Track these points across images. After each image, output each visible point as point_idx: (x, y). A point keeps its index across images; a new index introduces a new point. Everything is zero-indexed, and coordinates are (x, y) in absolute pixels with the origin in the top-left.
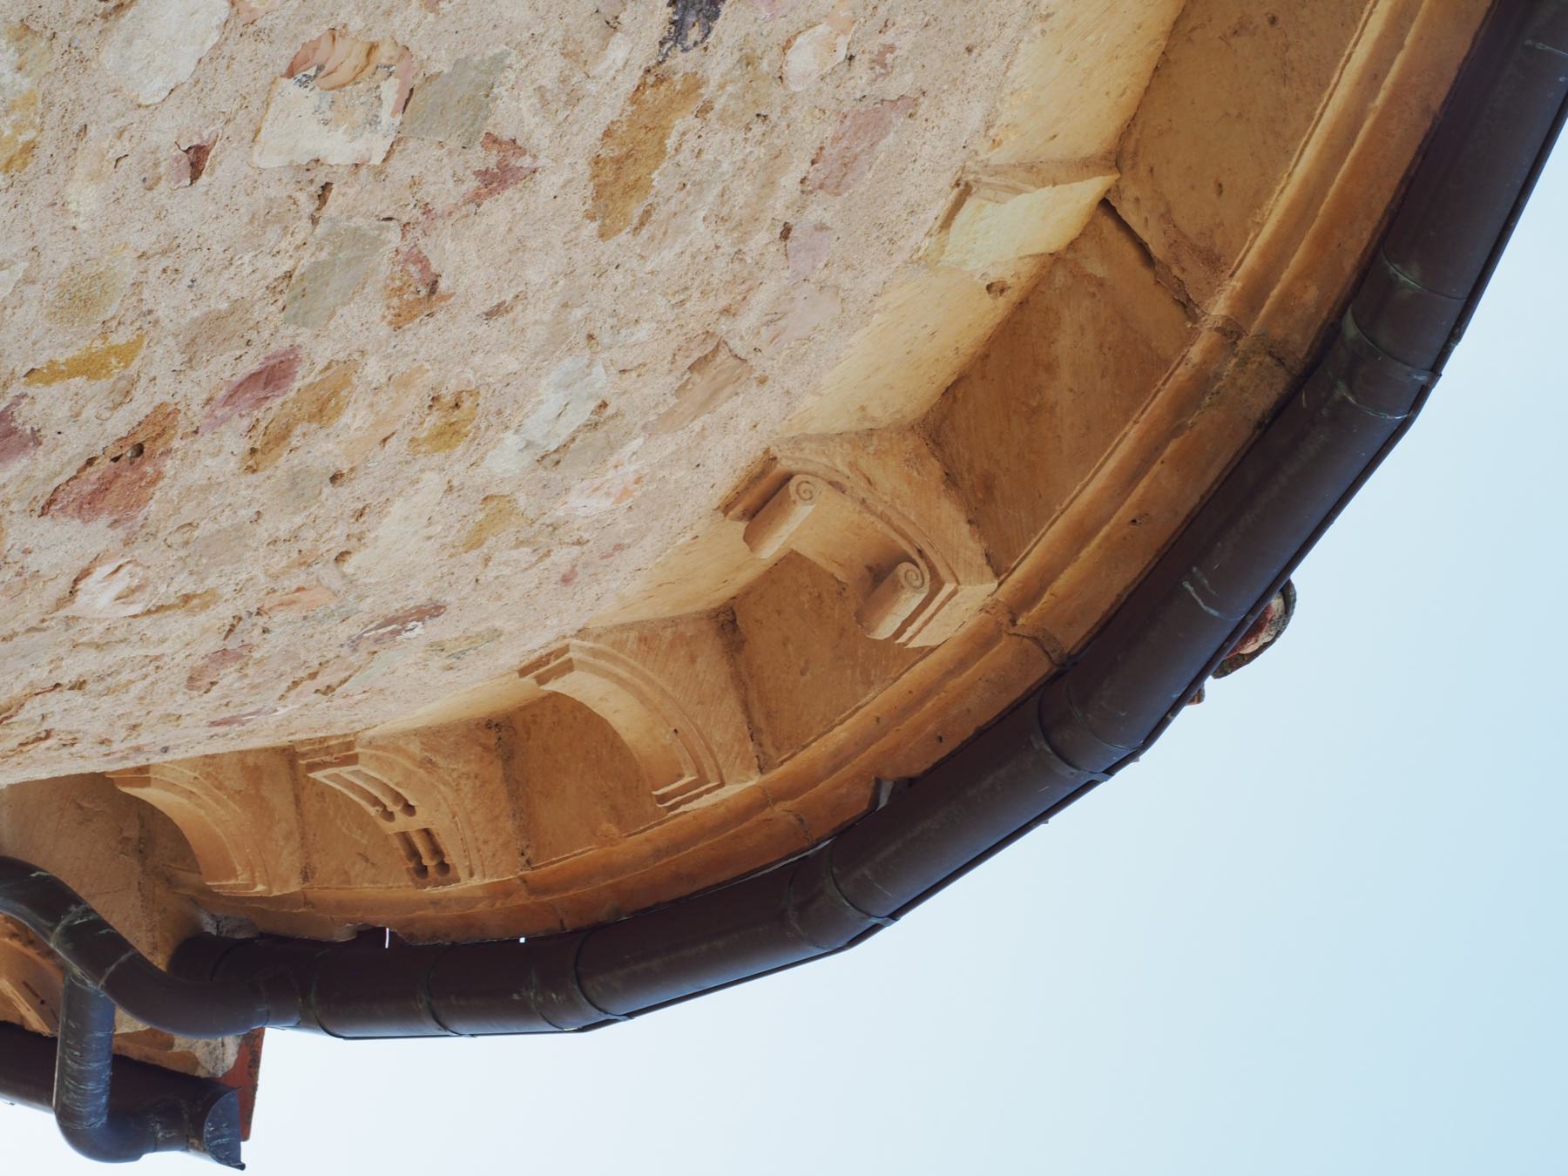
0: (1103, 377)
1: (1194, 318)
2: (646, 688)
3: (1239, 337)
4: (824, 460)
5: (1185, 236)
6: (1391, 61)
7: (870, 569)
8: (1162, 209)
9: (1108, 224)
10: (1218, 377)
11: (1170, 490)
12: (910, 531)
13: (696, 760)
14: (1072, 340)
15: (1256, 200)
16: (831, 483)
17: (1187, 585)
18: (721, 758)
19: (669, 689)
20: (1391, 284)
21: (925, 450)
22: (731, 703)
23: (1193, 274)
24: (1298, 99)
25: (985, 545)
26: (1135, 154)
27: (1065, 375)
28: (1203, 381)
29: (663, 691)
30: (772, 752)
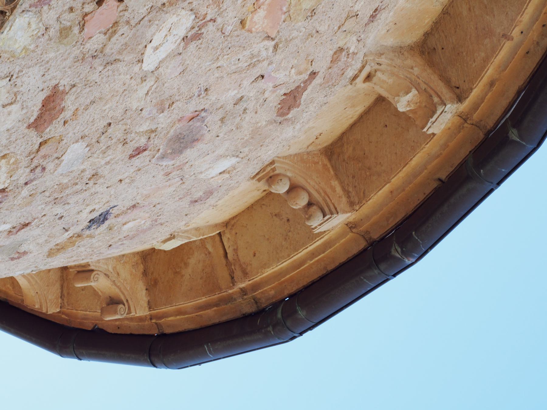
0: (201, 279)
1: (234, 285)
2: (31, 280)
3: (245, 295)
4: (106, 267)
5: (239, 260)
6: (320, 254)
7: (110, 297)
8: (235, 247)
9: (218, 238)
10: (235, 300)
11: (211, 316)
12: (126, 293)
13: (41, 303)
14: (195, 261)
15: (265, 266)
16: (105, 274)
17: (206, 346)
18: (49, 304)
19: (39, 281)
20: (296, 312)
21: (140, 262)
22: (58, 285)
23: (238, 273)
24: (287, 248)
25: (149, 298)
26: (233, 226)
27: (190, 270)
28: (230, 299)
29: (36, 282)
30: (66, 304)
